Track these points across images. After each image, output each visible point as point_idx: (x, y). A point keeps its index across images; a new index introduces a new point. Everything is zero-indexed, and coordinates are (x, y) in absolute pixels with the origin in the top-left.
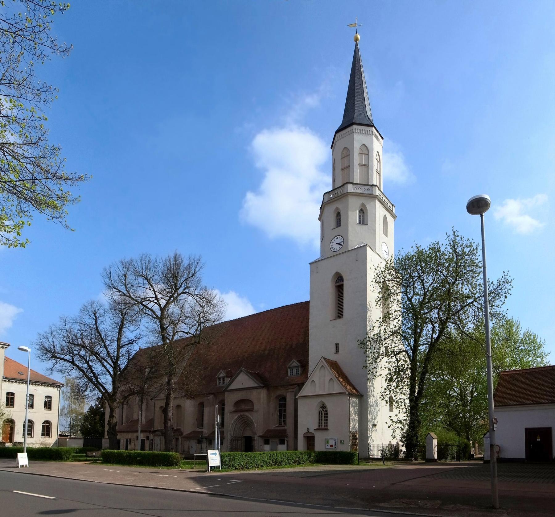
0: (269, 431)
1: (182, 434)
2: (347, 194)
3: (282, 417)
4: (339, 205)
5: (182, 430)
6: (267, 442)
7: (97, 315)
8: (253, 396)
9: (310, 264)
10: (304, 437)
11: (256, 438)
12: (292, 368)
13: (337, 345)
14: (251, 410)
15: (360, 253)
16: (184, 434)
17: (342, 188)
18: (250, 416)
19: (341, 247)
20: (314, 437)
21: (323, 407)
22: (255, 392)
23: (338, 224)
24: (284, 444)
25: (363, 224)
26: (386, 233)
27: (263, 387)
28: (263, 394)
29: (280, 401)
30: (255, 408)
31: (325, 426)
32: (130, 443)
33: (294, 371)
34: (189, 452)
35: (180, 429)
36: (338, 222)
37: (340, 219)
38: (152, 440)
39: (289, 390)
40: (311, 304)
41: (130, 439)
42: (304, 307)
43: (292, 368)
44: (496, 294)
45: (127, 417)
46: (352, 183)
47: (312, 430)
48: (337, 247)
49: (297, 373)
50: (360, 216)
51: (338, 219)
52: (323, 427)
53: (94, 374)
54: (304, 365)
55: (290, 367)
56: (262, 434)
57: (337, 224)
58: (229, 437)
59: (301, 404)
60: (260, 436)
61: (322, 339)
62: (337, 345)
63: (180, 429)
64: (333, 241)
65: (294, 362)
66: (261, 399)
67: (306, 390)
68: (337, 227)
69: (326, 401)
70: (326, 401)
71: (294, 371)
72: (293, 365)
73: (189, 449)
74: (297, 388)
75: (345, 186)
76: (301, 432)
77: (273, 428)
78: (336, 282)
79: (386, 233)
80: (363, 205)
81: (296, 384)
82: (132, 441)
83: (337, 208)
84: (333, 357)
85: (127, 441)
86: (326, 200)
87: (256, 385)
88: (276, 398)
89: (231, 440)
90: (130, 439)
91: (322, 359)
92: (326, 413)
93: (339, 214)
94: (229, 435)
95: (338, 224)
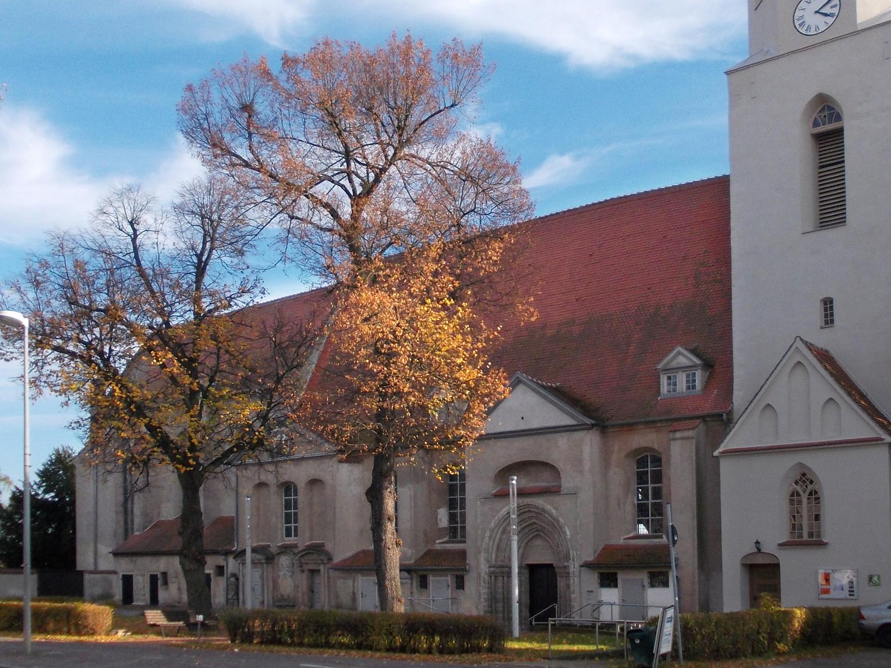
0: (609, 550)
1: (330, 559)
5: (329, 547)
8: (558, 450)
9: (728, 73)
10: (744, 565)
11: (574, 567)
12: (671, 371)
13: (828, 304)
14: (552, 491)
16: (336, 560)
18: (548, 507)
19: (830, 20)
20: (777, 566)
21: (805, 478)
22: (563, 441)
24: (665, 584)
27: (593, 425)
28: (589, 443)
30: (567, 483)
31: (811, 535)
32: (166, 583)
34: (354, 608)
38: (234, 575)
39: (678, 435)
40: (735, 189)
41: (165, 574)
42: (711, 198)
43: (671, 371)
45: (145, 515)
47: (770, 546)
48: (821, 23)
49: (691, 386)
52: (805, 537)
53: (423, 160)
55: (666, 370)
56: (591, 559)
58: (484, 568)
60: (588, 565)
62: (828, 304)
65: (679, 353)
69: (815, 462)
72: (674, 364)
73: (354, 599)
74: (701, 426)
76: (733, 554)
77: (621, 542)
78: (816, 124)
81: (698, 417)
84: (823, 339)
85: (154, 579)
88: (628, 455)
89: (490, 574)
90: (165, 574)
91: (799, 344)
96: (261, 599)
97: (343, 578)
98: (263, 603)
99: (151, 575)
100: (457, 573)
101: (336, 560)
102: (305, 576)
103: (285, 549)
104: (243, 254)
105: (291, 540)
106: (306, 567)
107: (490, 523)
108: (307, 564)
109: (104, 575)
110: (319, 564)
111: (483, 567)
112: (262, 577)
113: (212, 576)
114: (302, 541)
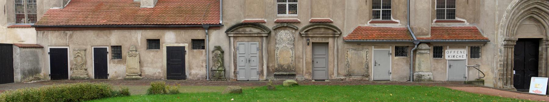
16: (345, 35)
96: (258, 69)
97: (355, 50)
98: (429, 50)
99: (96, 50)
100: (473, 45)
101: (345, 35)
102: (309, 48)
103: (282, 25)
104: (483, 82)
105: (288, 16)
106: (312, 41)
107: (507, 6)
108: (312, 37)
109: (34, 49)
110: (328, 37)
111: (500, 40)
112: (261, 49)
113: (186, 49)
114: (303, 18)
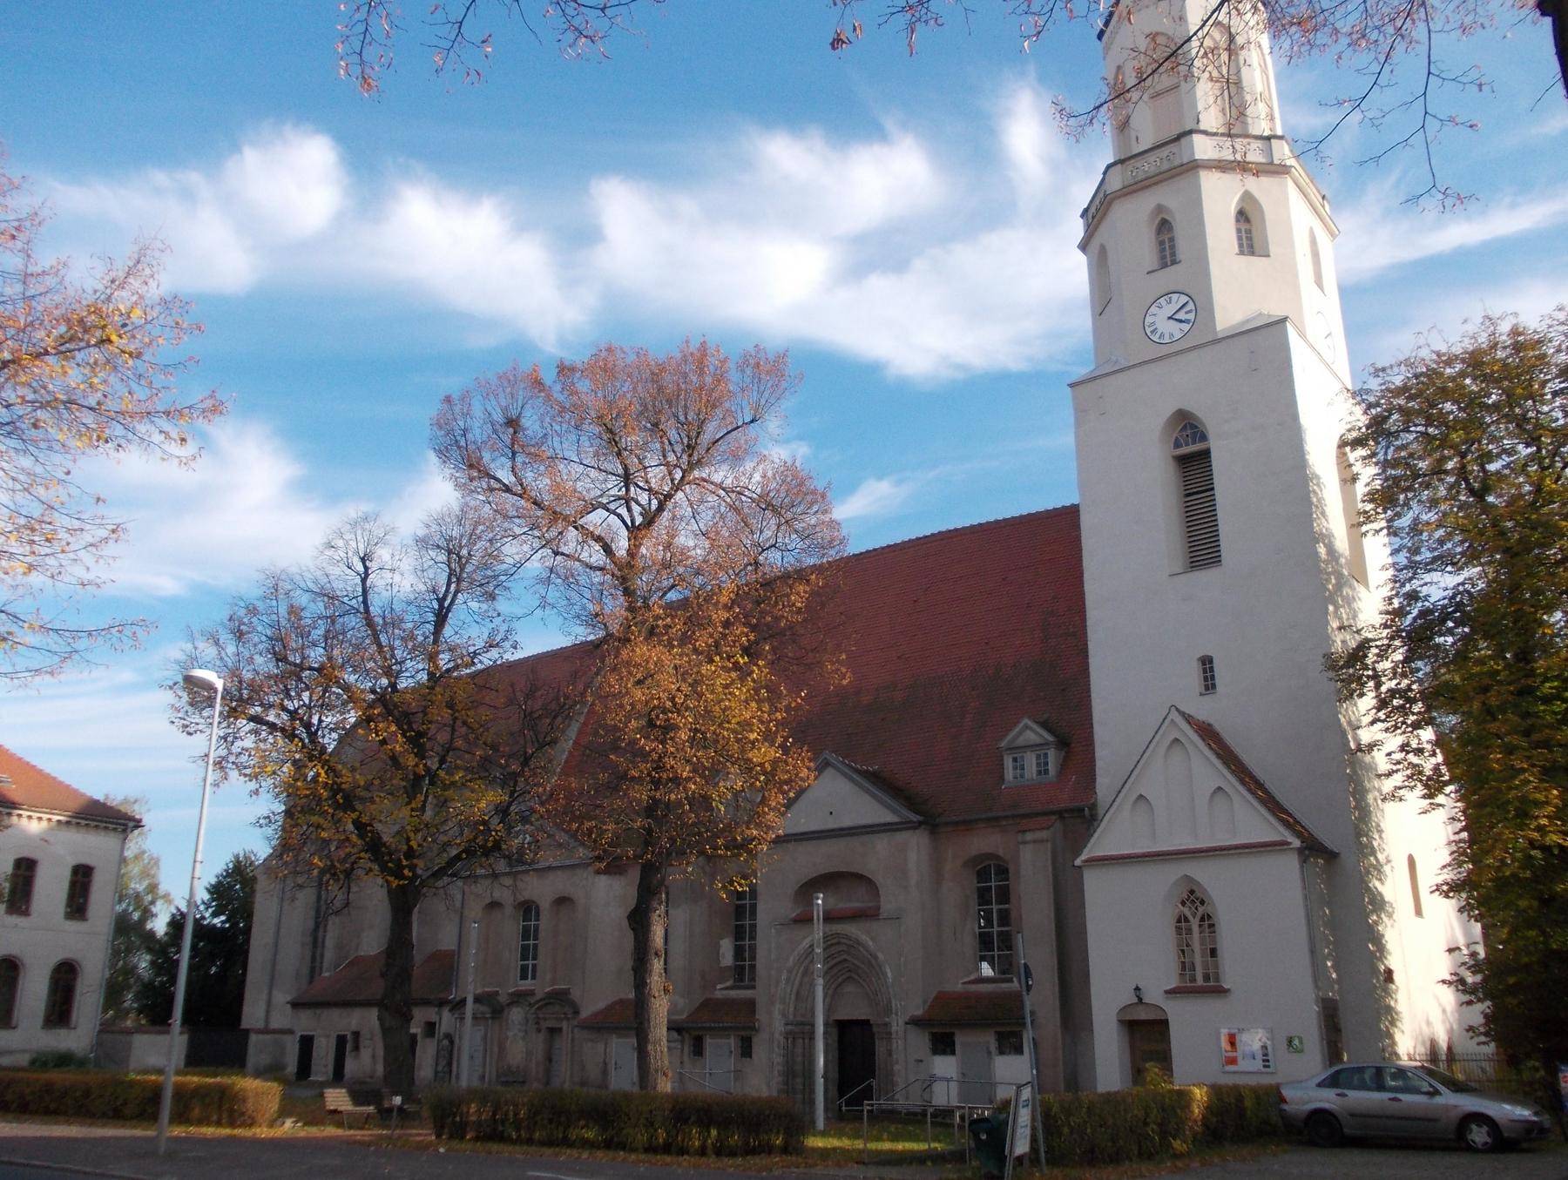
0: (943, 999)
1: (576, 1012)
2: (1194, 166)
3: (996, 942)
4: (1166, 196)
5: (576, 994)
6: (943, 1044)
7: (373, 565)
8: (875, 857)
10: (1121, 1022)
11: (897, 1024)
13: (1207, 663)
14: (868, 915)
15: (1266, 341)
16: (584, 1014)
17: (1172, 148)
18: (864, 938)
20: (1164, 1023)
21: (1193, 897)
23: (1167, 254)
24: (1019, 1050)
25: (1252, 253)
26: (1319, 282)
28: (916, 845)
29: (983, 875)
30: (888, 904)
31: (1207, 978)
32: (356, 1048)
33: (1030, 760)
34: (604, 1085)
35: (566, 992)
36: (1162, 250)
37: (1172, 239)
38: (449, 1037)
39: (1029, 836)
40: (1086, 521)
41: (356, 1034)
44: (332, 598)
46: (1205, 133)
47: (1154, 996)
48: (1176, 330)
49: (1043, 771)
50: (1239, 231)
51: (1162, 243)
52: (1200, 981)
54: (1073, 738)
55: (1010, 749)
56: (919, 1012)
57: (1163, 257)
58: (779, 1026)
59: (1099, 890)
60: (915, 1022)
61: (1139, 635)
62: (1207, 663)
63: (566, 992)
64: (1153, 309)
65: (1027, 727)
66: (906, 867)
67: (1109, 839)
68: (1164, 266)
69: (1206, 874)
70: (1206, 874)
71: (1030, 760)
72: (1020, 741)
73: (605, 1073)
75: (1184, 141)
76: (1106, 1003)
77: (959, 988)
78: (1177, 445)
79: (1319, 282)
80: (1247, 197)
81: (1053, 813)
82: (364, 1042)
83: (1160, 208)
84: (1203, 709)
85: (341, 1041)
86: (1115, 183)
87: (889, 817)
88: (966, 864)
89: (787, 1035)
90: (356, 1034)
91: (1174, 715)
92: (1208, 922)
93: (1164, 226)
94: (777, 1015)
95: (1167, 254)
